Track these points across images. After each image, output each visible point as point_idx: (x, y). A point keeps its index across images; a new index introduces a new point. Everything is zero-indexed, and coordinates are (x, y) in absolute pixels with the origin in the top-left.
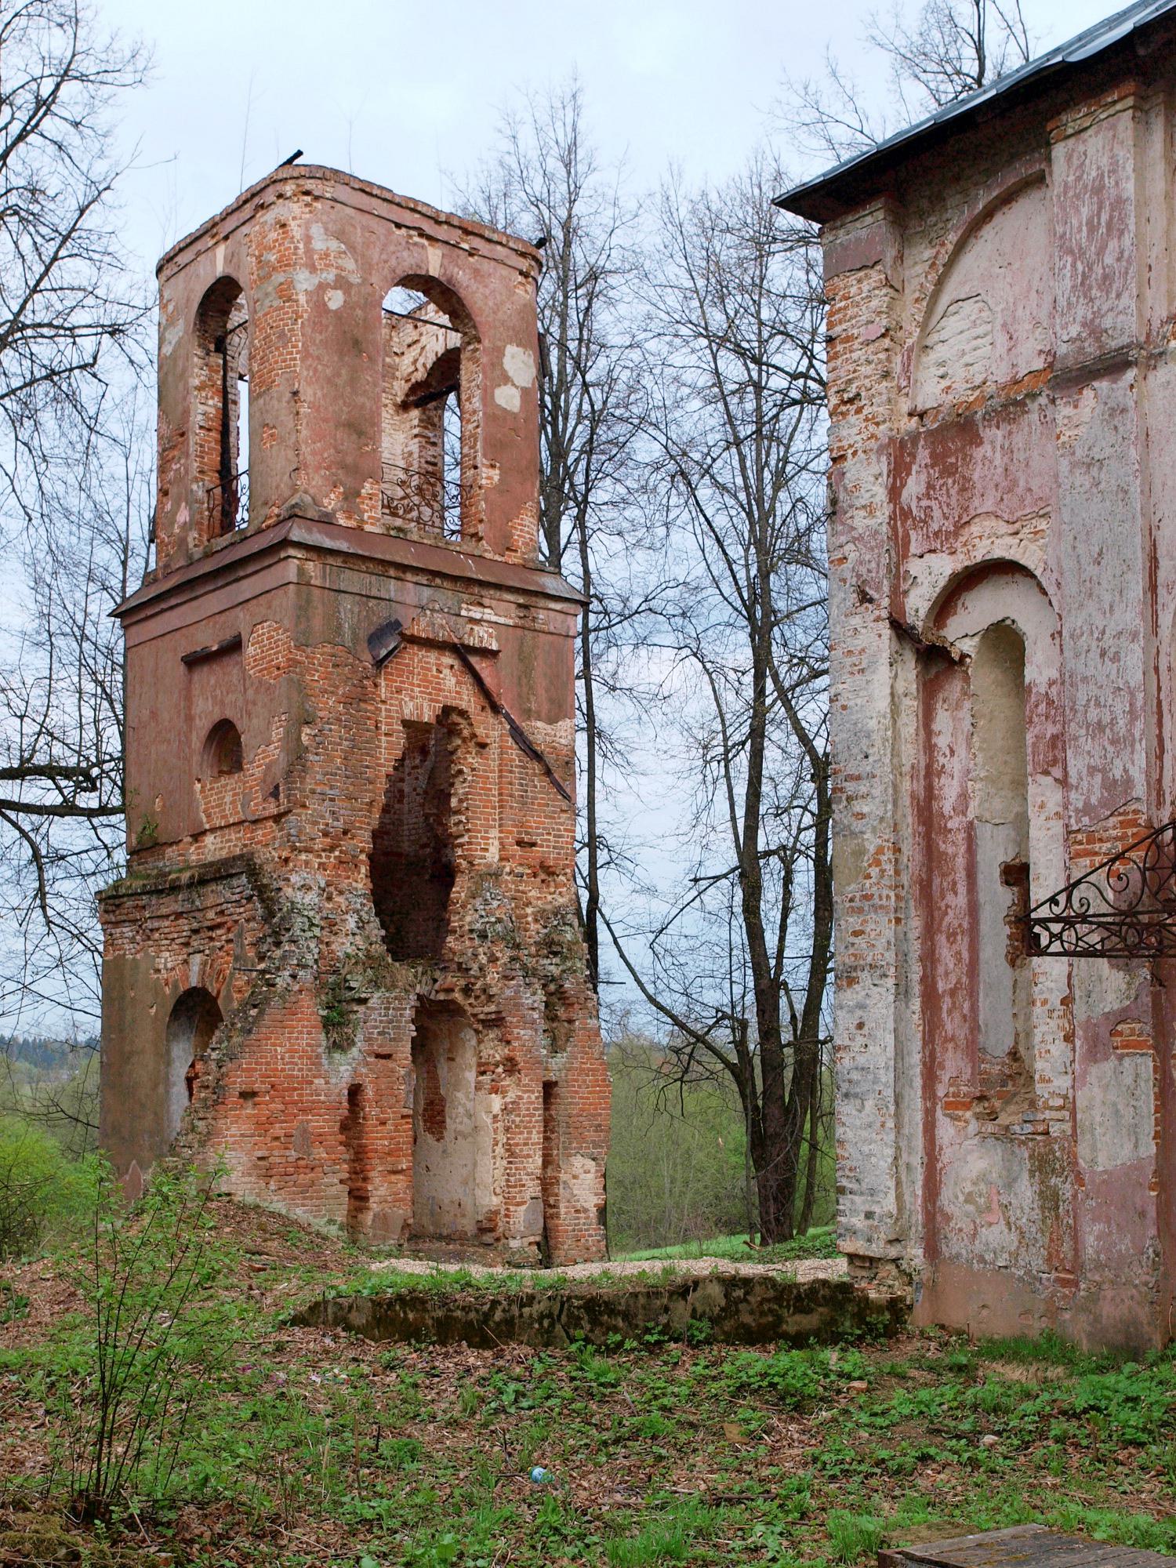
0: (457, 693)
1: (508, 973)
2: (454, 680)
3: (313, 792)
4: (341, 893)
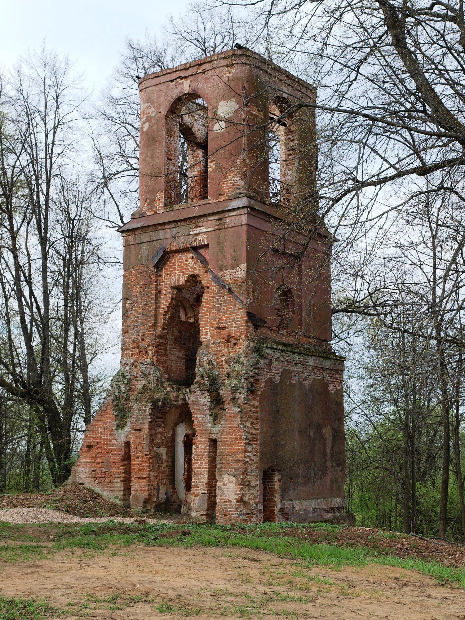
0: (195, 268)
2: (193, 263)
3: (130, 326)
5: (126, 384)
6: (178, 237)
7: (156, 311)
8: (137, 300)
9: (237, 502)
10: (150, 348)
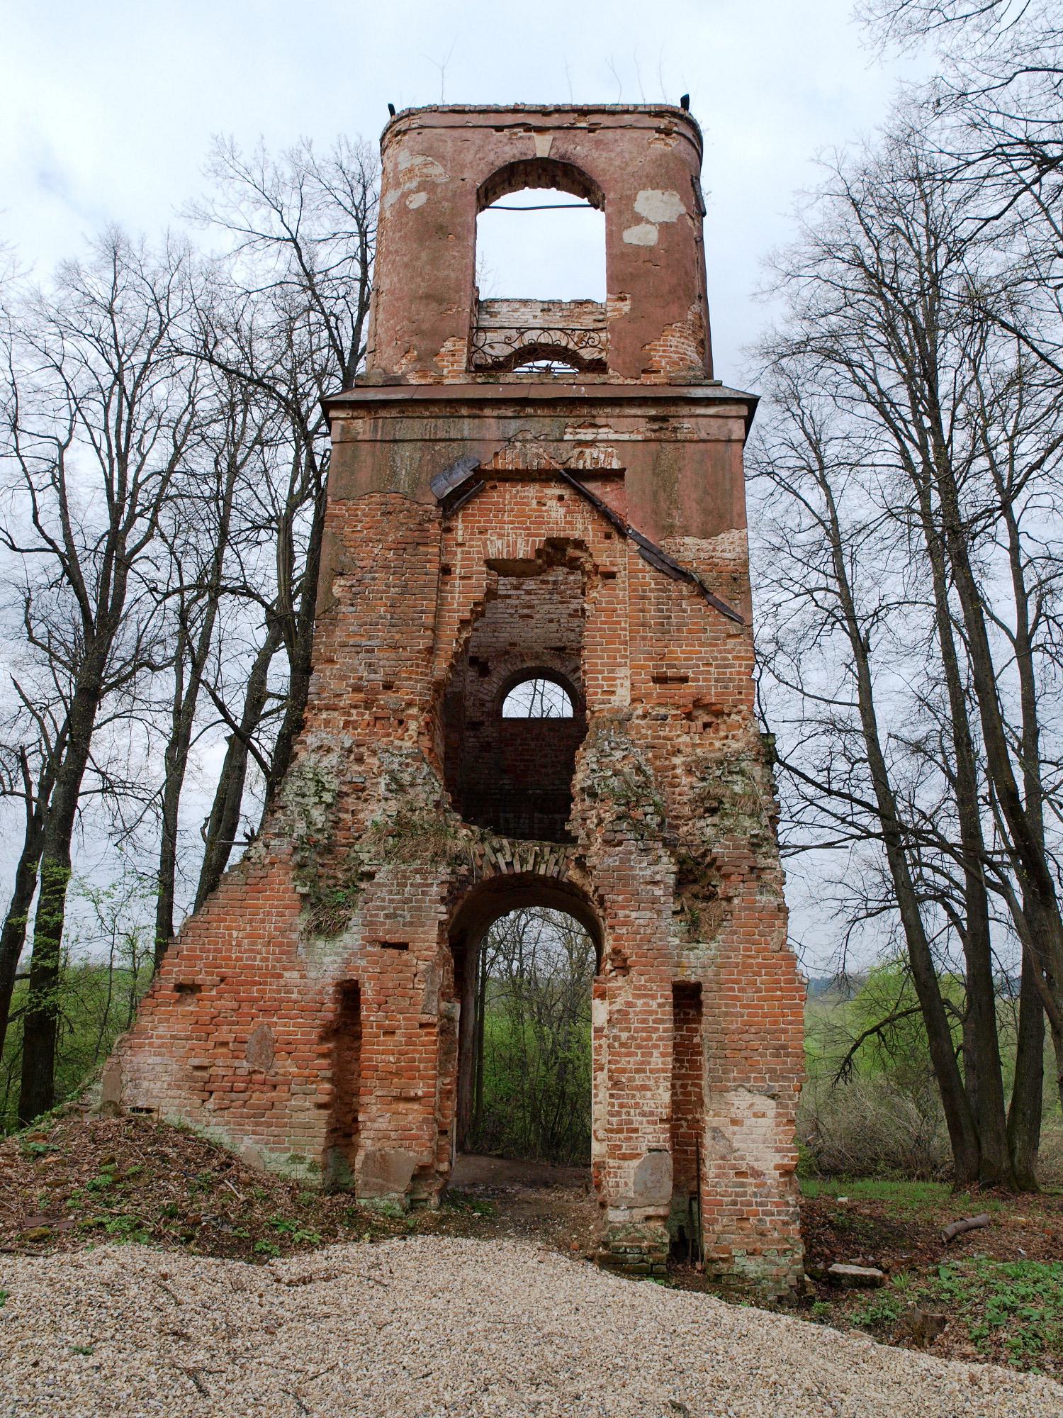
0: (567, 522)
1: (610, 836)
2: (562, 511)
3: (344, 645)
4: (374, 753)
5: (329, 806)
6: (524, 441)
7: (437, 615)
8: (374, 579)
9: (781, 1175)
10: (414, 711)
